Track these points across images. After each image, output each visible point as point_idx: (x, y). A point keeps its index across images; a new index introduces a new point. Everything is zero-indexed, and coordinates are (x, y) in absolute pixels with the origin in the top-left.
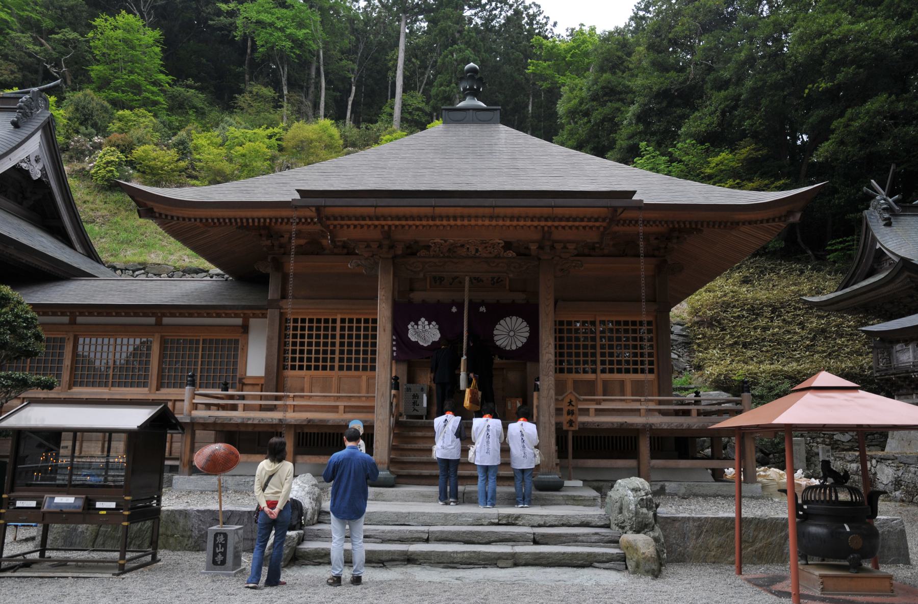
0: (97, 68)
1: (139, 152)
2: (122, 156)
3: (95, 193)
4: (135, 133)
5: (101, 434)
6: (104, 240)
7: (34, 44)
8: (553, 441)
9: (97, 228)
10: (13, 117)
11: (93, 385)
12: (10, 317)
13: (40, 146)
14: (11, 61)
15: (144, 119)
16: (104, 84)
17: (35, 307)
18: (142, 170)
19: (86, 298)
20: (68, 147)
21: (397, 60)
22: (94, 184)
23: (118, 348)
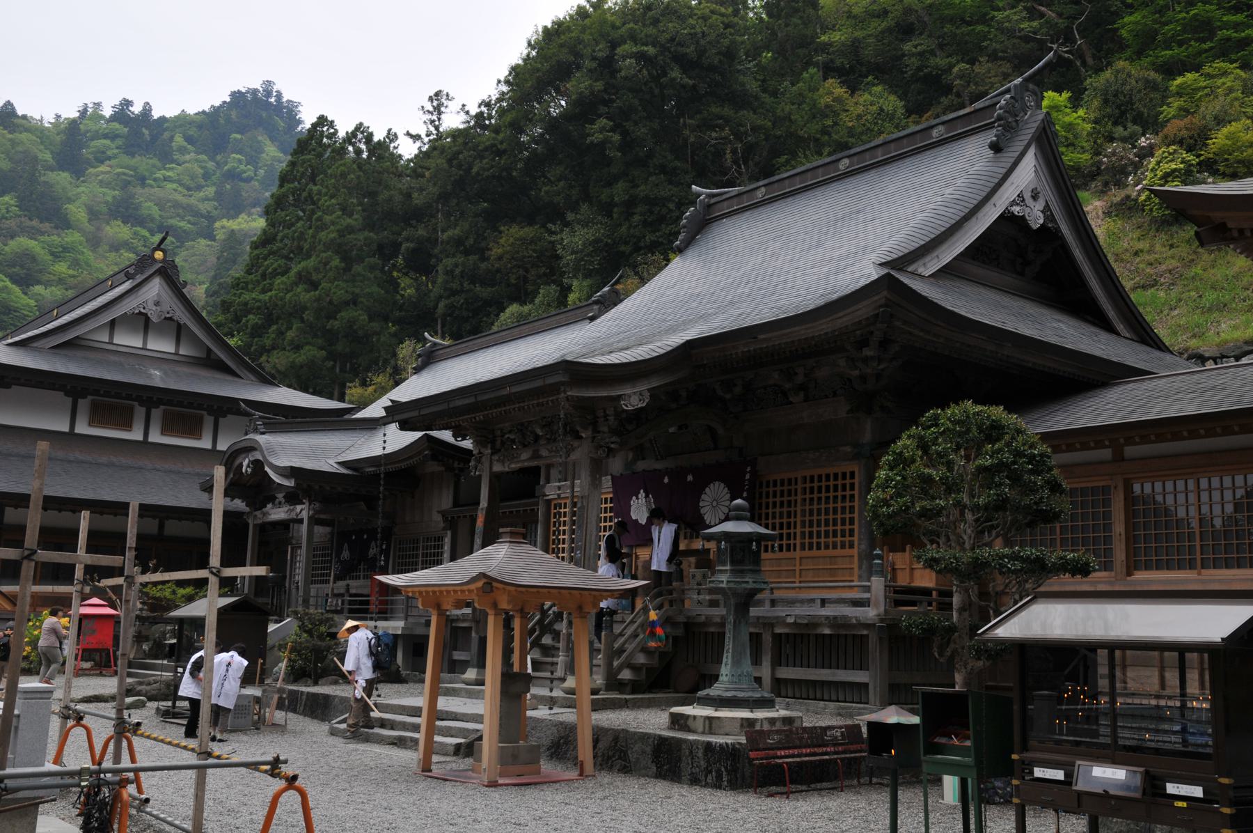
0: (1131, 18)
1: (1219, 139)
2: (1190, 157)
3: (1152, 233)
4: (1210, 109)
5: (1156, 653)
6: (1176, 312)
7: (1031, 19)
8: (676, 340)
9: (1162, 294)
10: (990, 136)
11: (1169, 566)
12: (1007, 457)
13: (1036, 171)
14: (1003, 59)
15: (1223, 80)
16: (1146, 41)
17: (1045, 437)
18: (1228, 171)
19: (1134, 412)
20: (1099, 168)
22: (1148, 219)
23: (1205, 497)
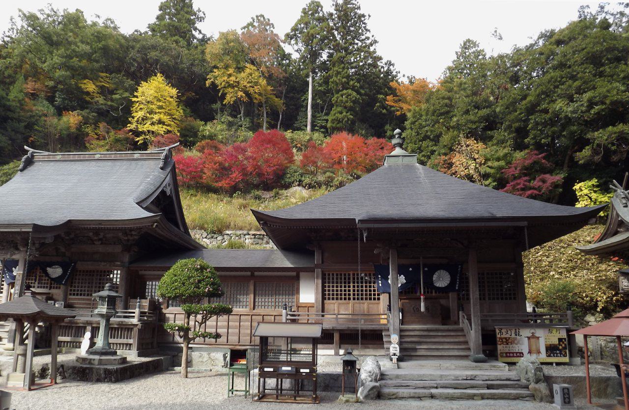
21: (308, 99)
